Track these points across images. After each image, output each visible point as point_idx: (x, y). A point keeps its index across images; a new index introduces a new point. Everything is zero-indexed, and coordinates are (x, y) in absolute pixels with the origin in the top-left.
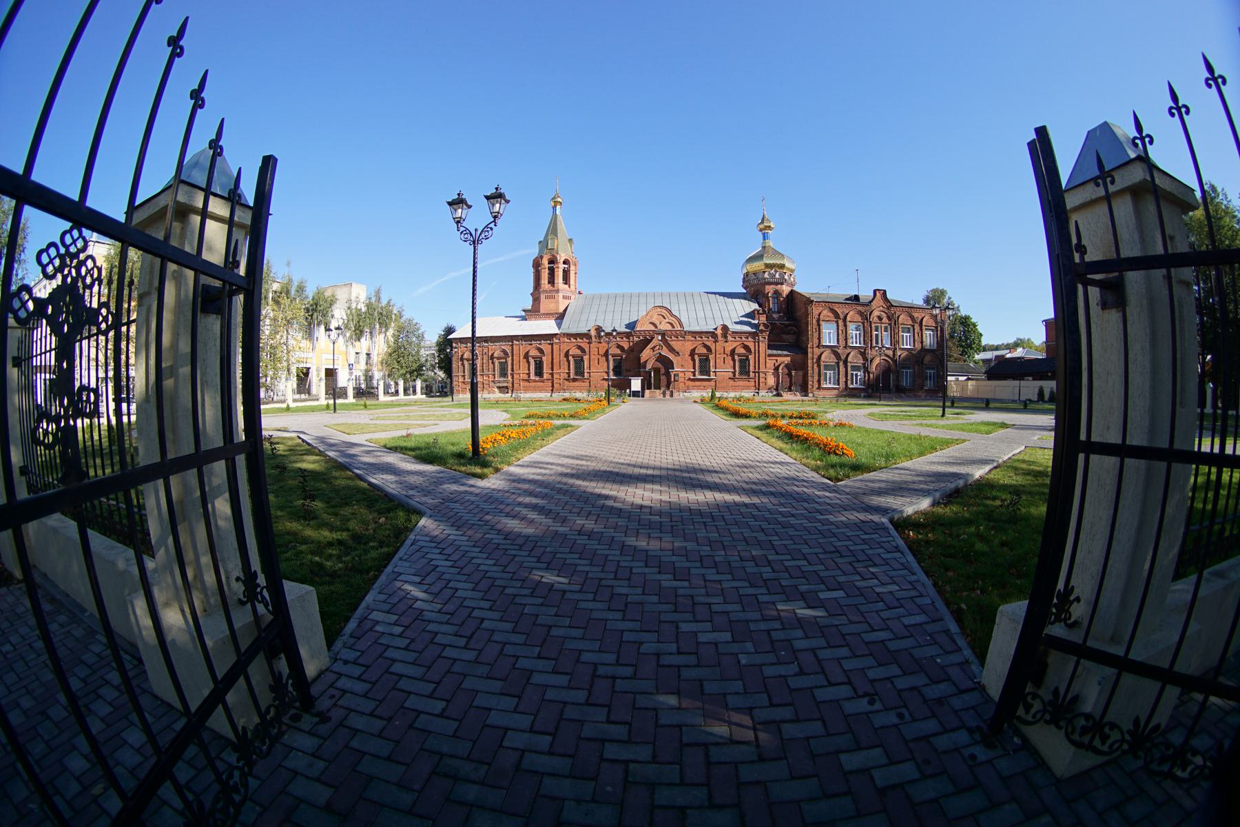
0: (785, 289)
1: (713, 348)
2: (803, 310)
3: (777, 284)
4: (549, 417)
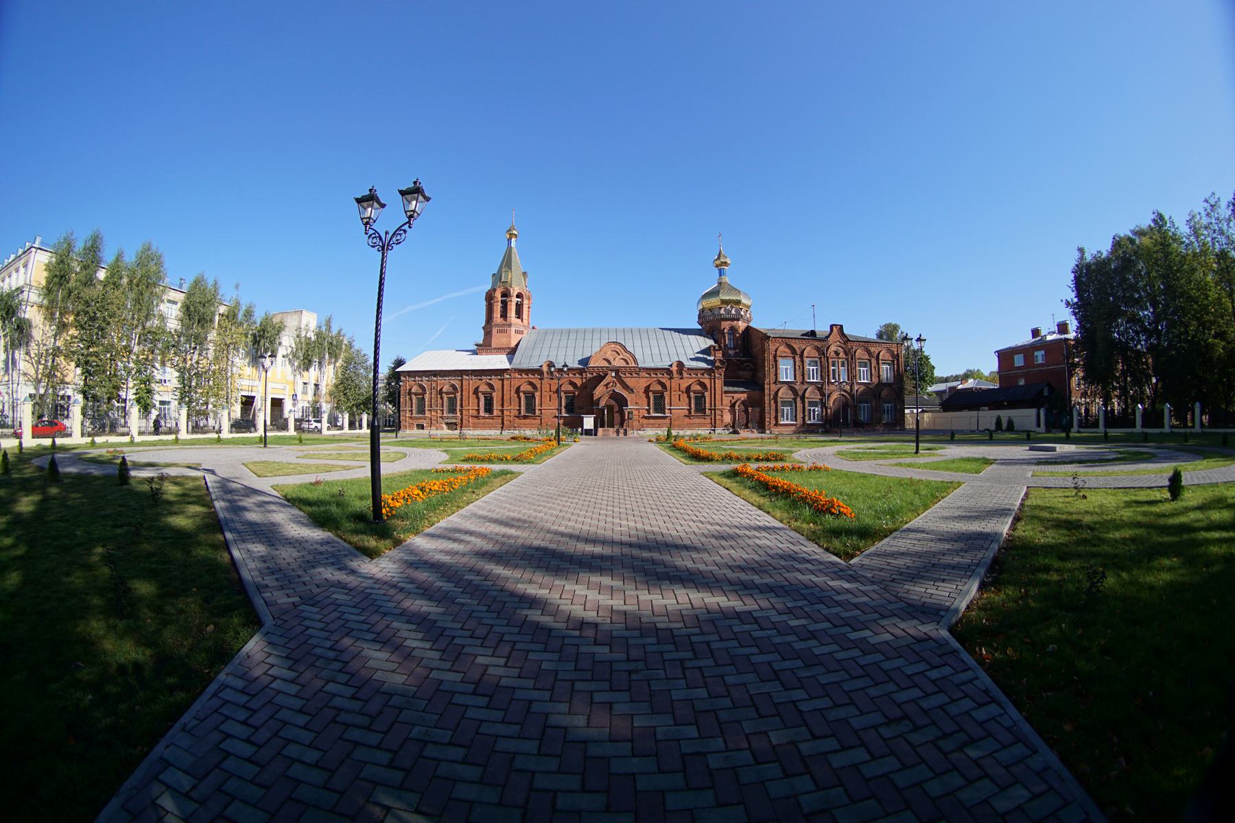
0: (741, 325)
1: (668, 385)
2: (759, 347)
3: (733, 320)
4: (490, 461)
